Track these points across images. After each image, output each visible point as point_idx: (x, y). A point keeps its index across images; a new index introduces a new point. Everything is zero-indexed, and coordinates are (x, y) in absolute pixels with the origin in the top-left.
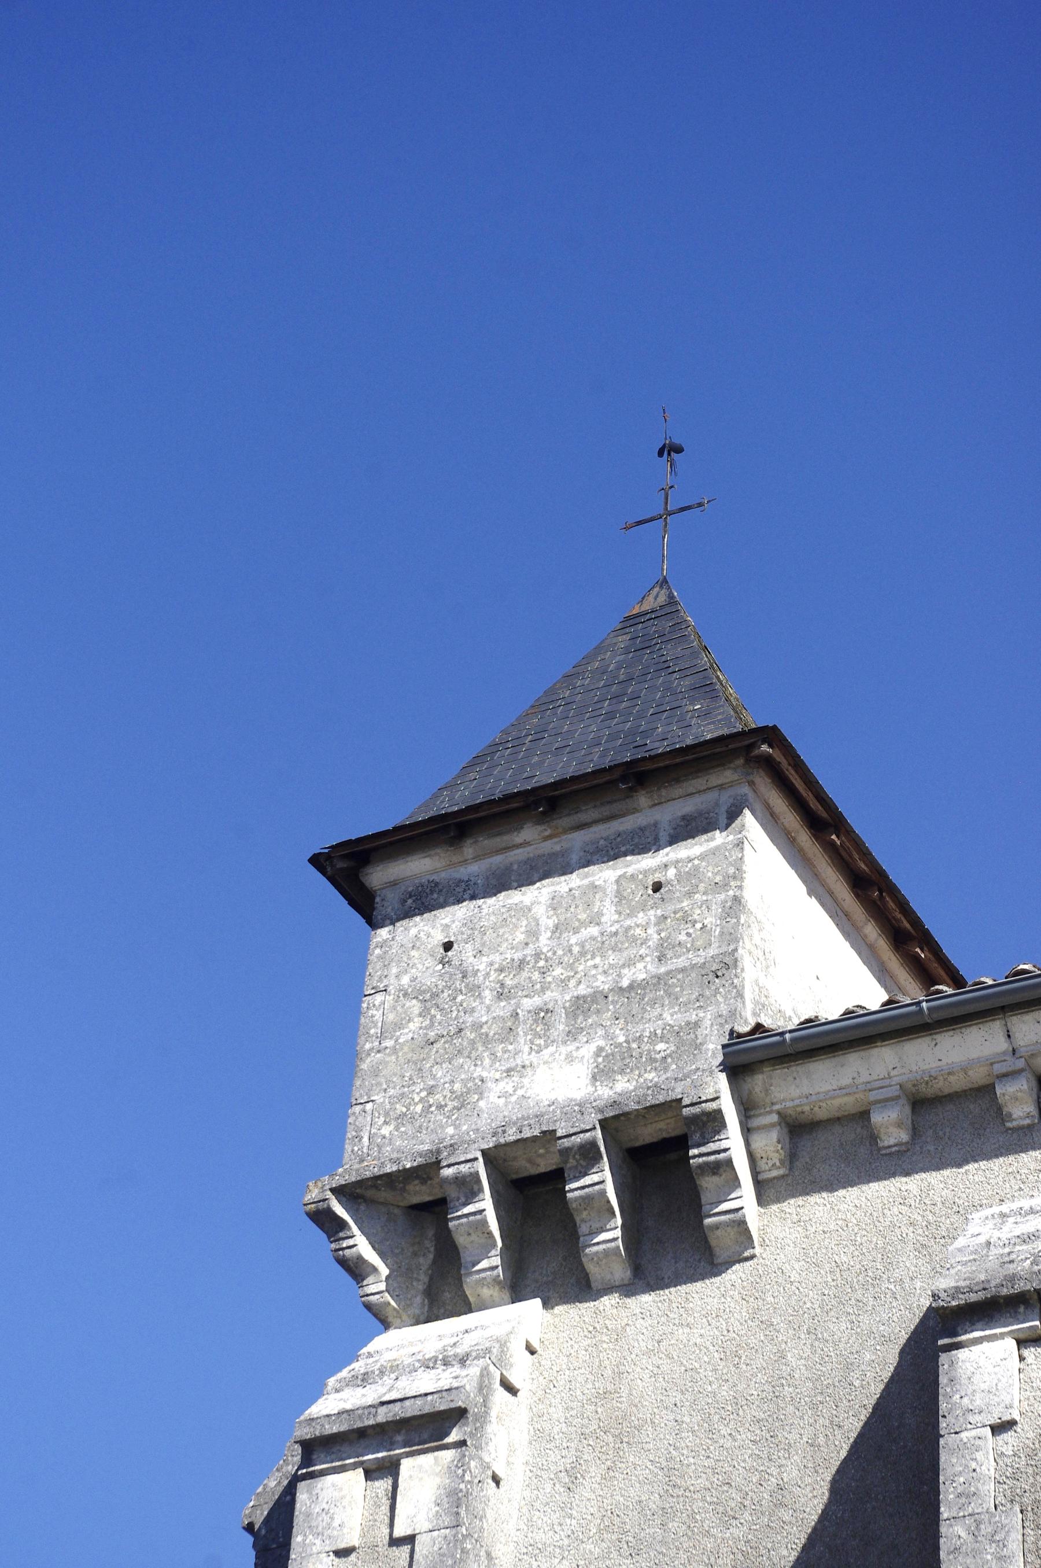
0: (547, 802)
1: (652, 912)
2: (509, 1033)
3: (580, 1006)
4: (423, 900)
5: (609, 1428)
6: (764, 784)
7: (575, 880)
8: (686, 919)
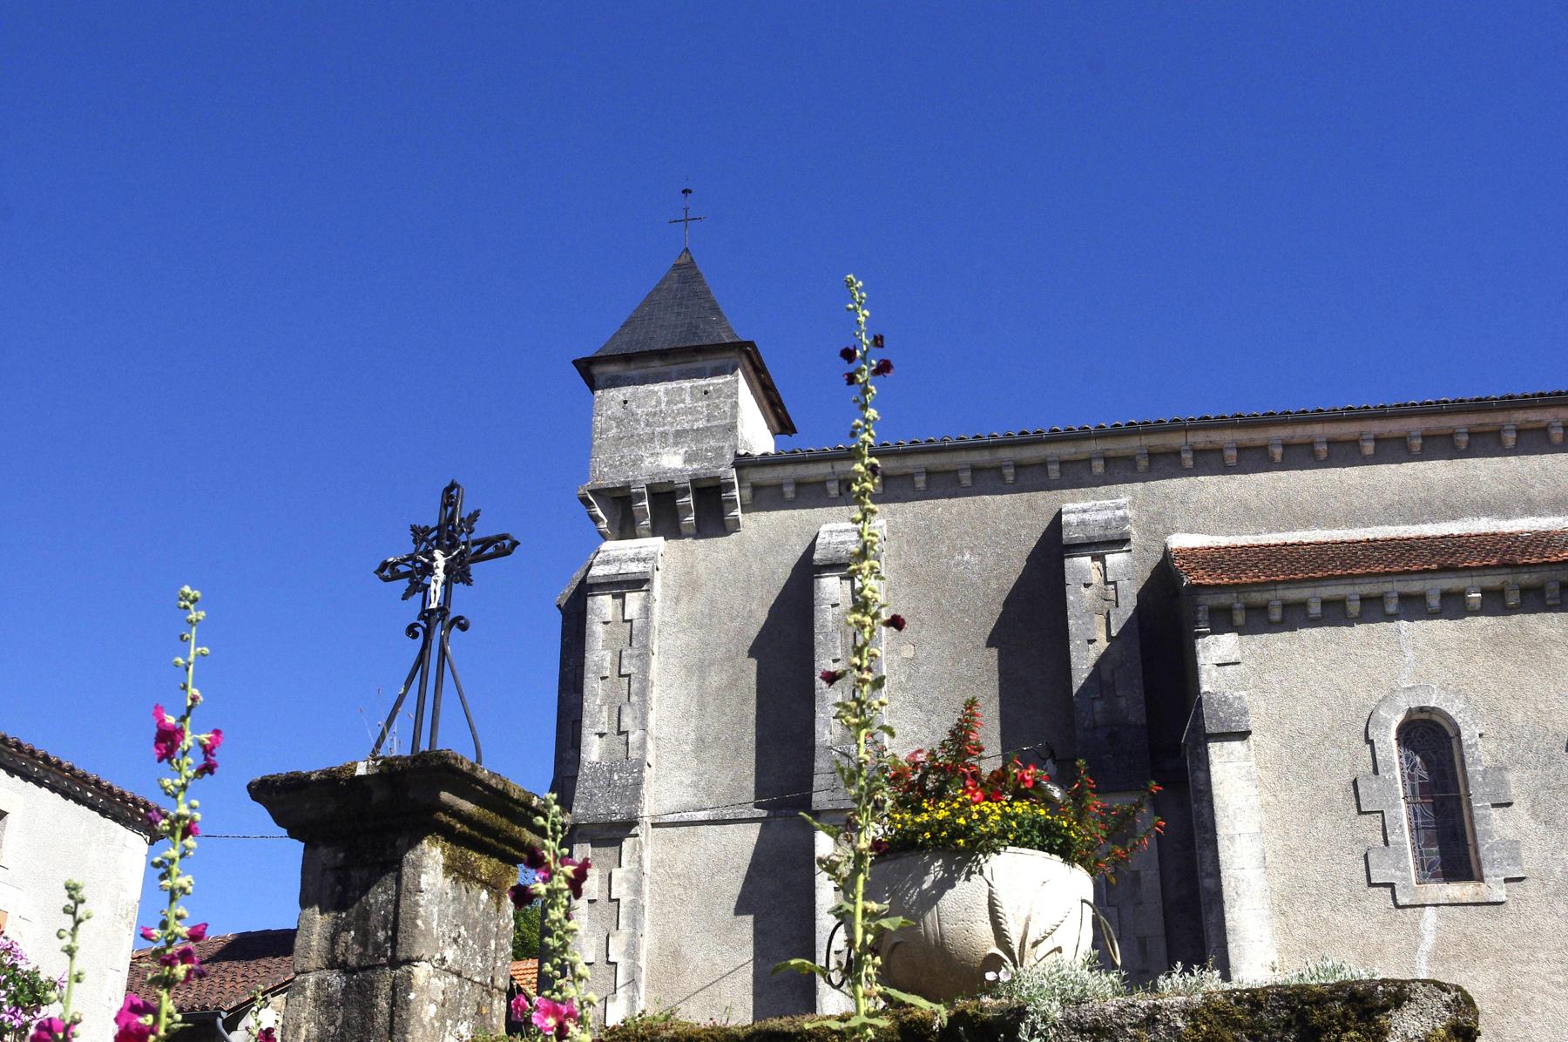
0: (663, 354)
1: (1119, 693)
2: (651, 440)
3: (678, 434)
4: (615, 382)
5: (689, 584)
6: (744, 357)
7: (674, 385)
8: (717, 407)
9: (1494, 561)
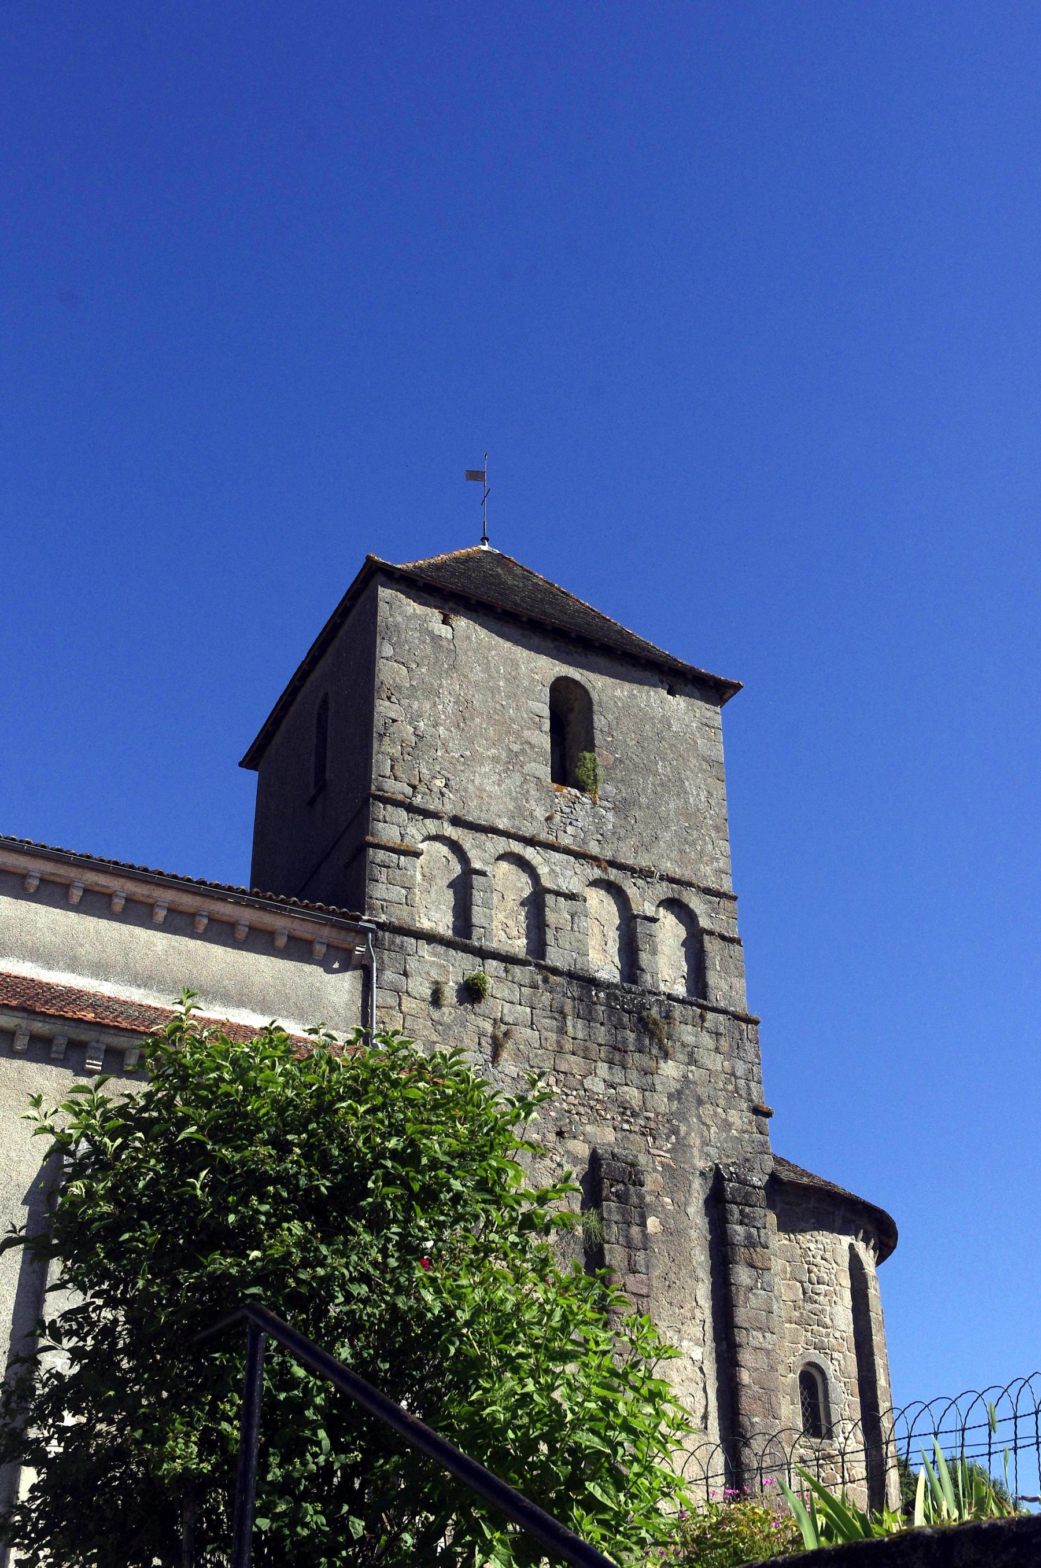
9: (14, 1003)
